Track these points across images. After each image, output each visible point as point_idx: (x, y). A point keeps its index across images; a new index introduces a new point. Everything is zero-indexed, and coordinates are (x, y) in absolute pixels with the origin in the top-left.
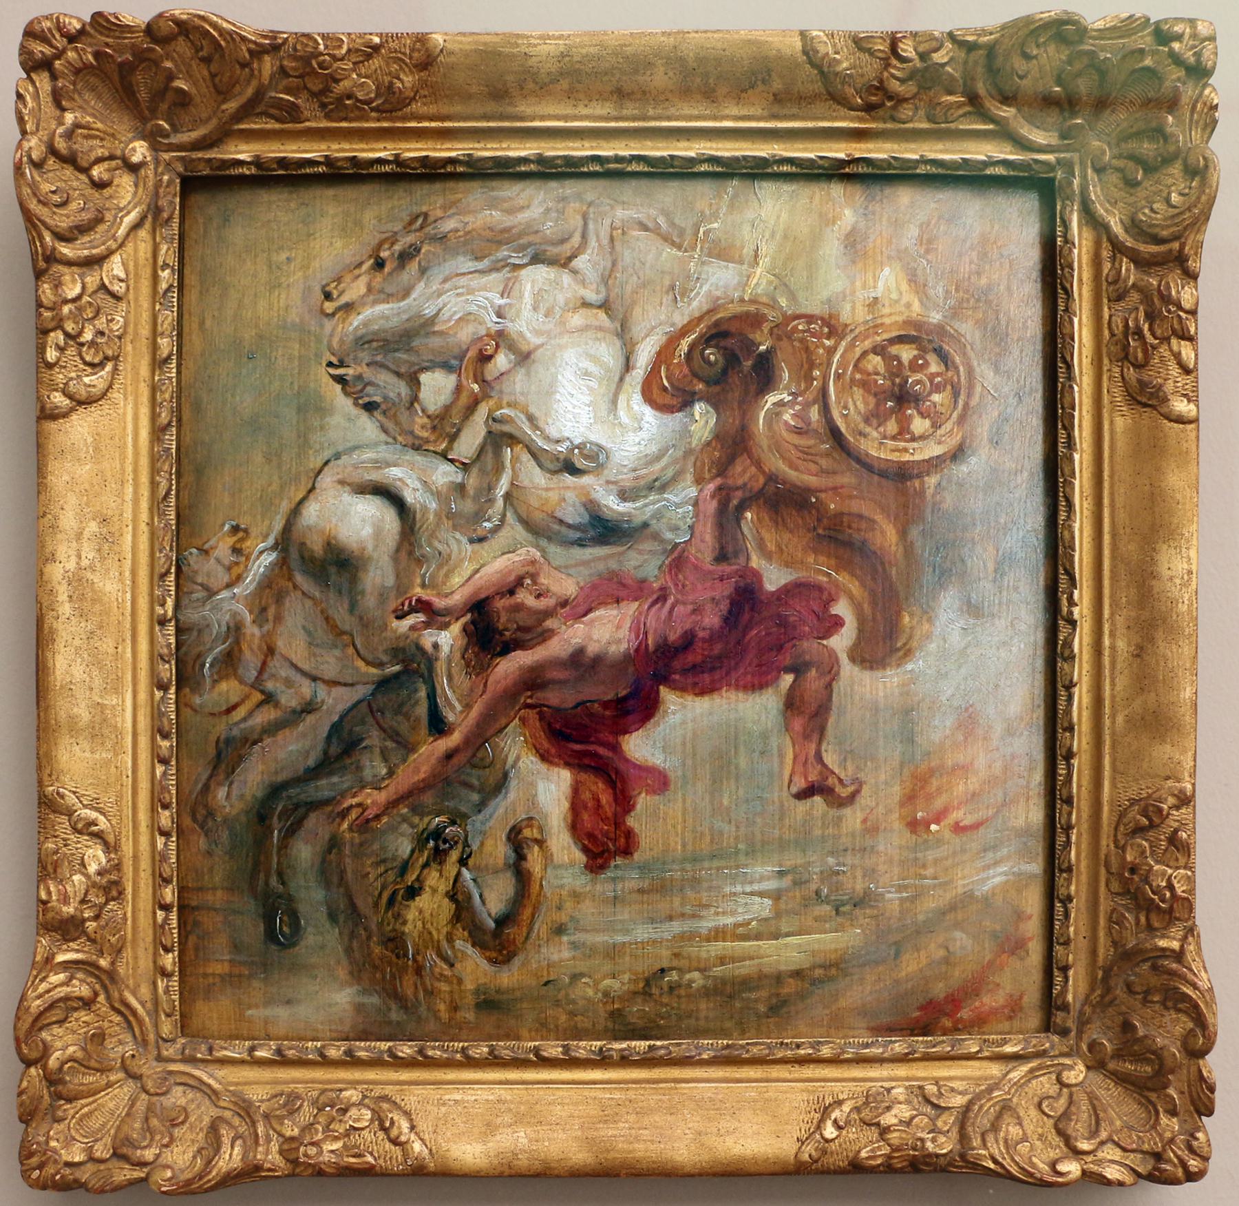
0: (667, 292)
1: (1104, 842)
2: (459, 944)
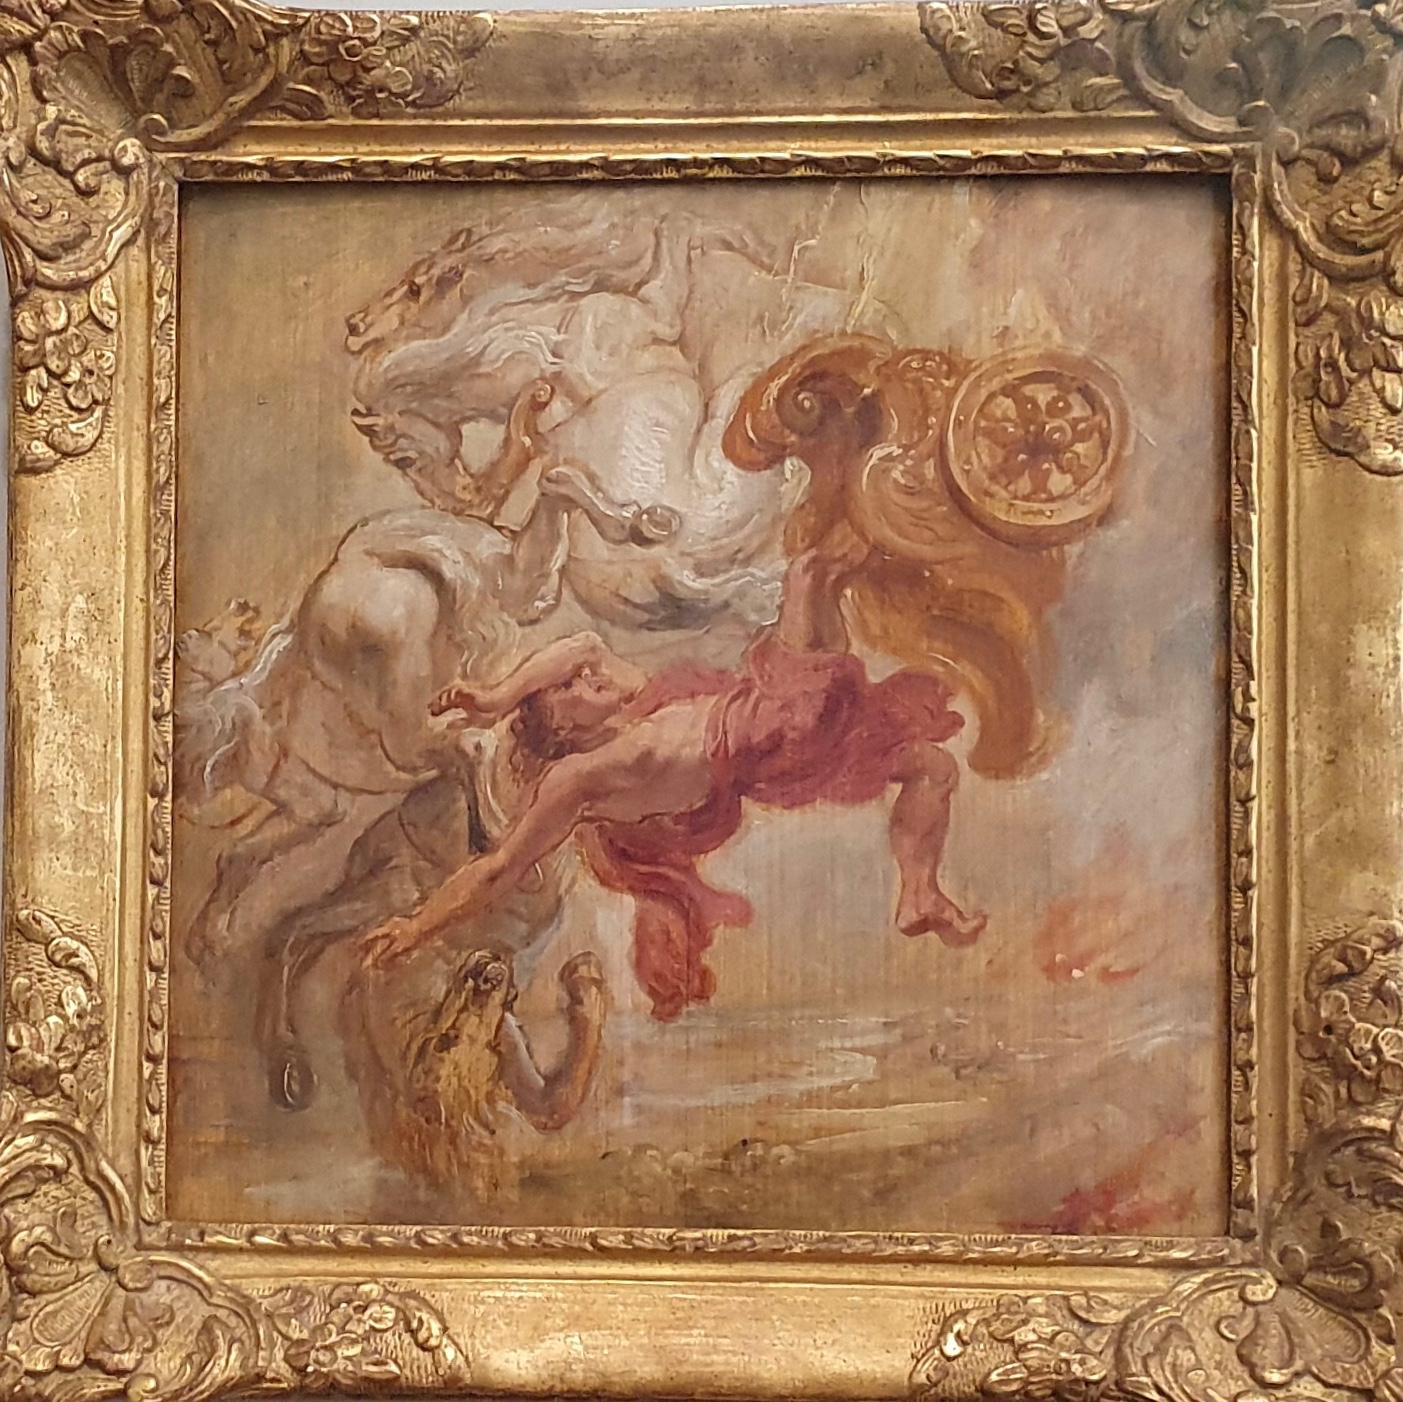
0: (755, 324)
1: (1292, 995)
2: (501, 1106)
